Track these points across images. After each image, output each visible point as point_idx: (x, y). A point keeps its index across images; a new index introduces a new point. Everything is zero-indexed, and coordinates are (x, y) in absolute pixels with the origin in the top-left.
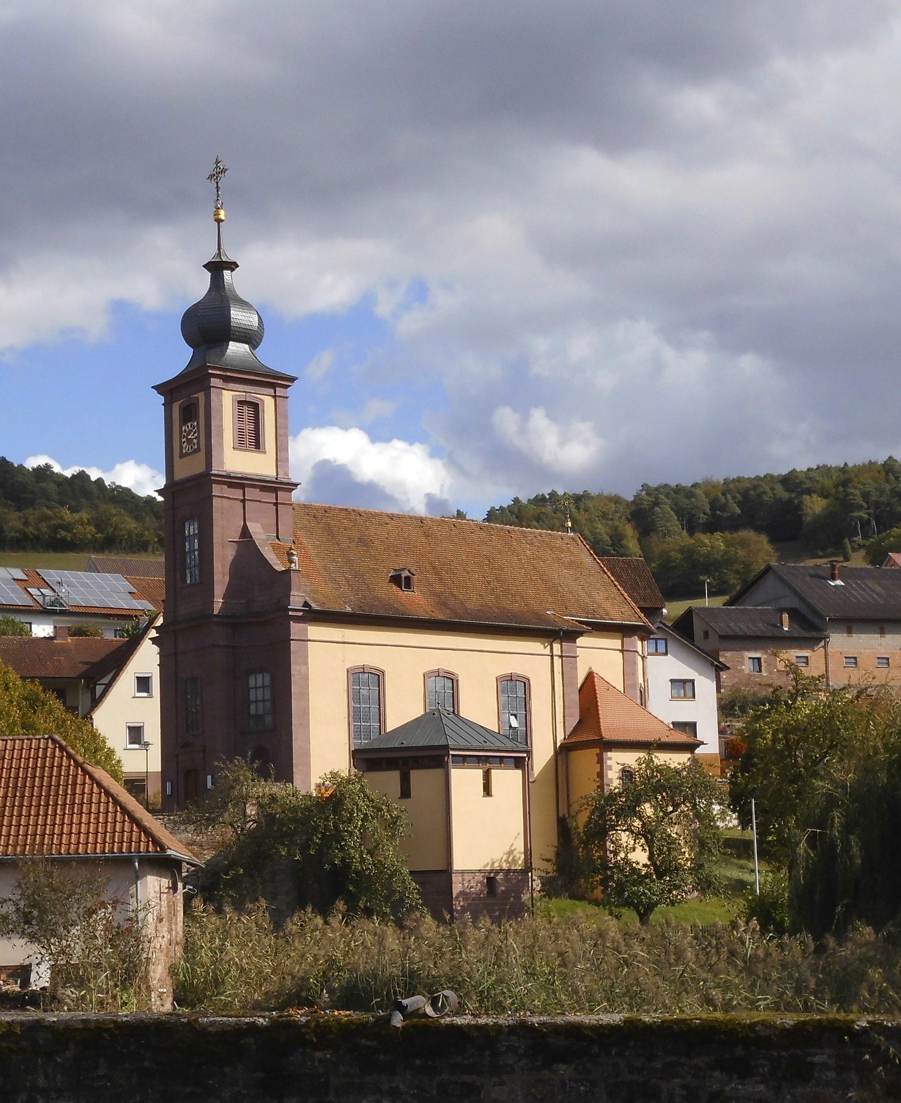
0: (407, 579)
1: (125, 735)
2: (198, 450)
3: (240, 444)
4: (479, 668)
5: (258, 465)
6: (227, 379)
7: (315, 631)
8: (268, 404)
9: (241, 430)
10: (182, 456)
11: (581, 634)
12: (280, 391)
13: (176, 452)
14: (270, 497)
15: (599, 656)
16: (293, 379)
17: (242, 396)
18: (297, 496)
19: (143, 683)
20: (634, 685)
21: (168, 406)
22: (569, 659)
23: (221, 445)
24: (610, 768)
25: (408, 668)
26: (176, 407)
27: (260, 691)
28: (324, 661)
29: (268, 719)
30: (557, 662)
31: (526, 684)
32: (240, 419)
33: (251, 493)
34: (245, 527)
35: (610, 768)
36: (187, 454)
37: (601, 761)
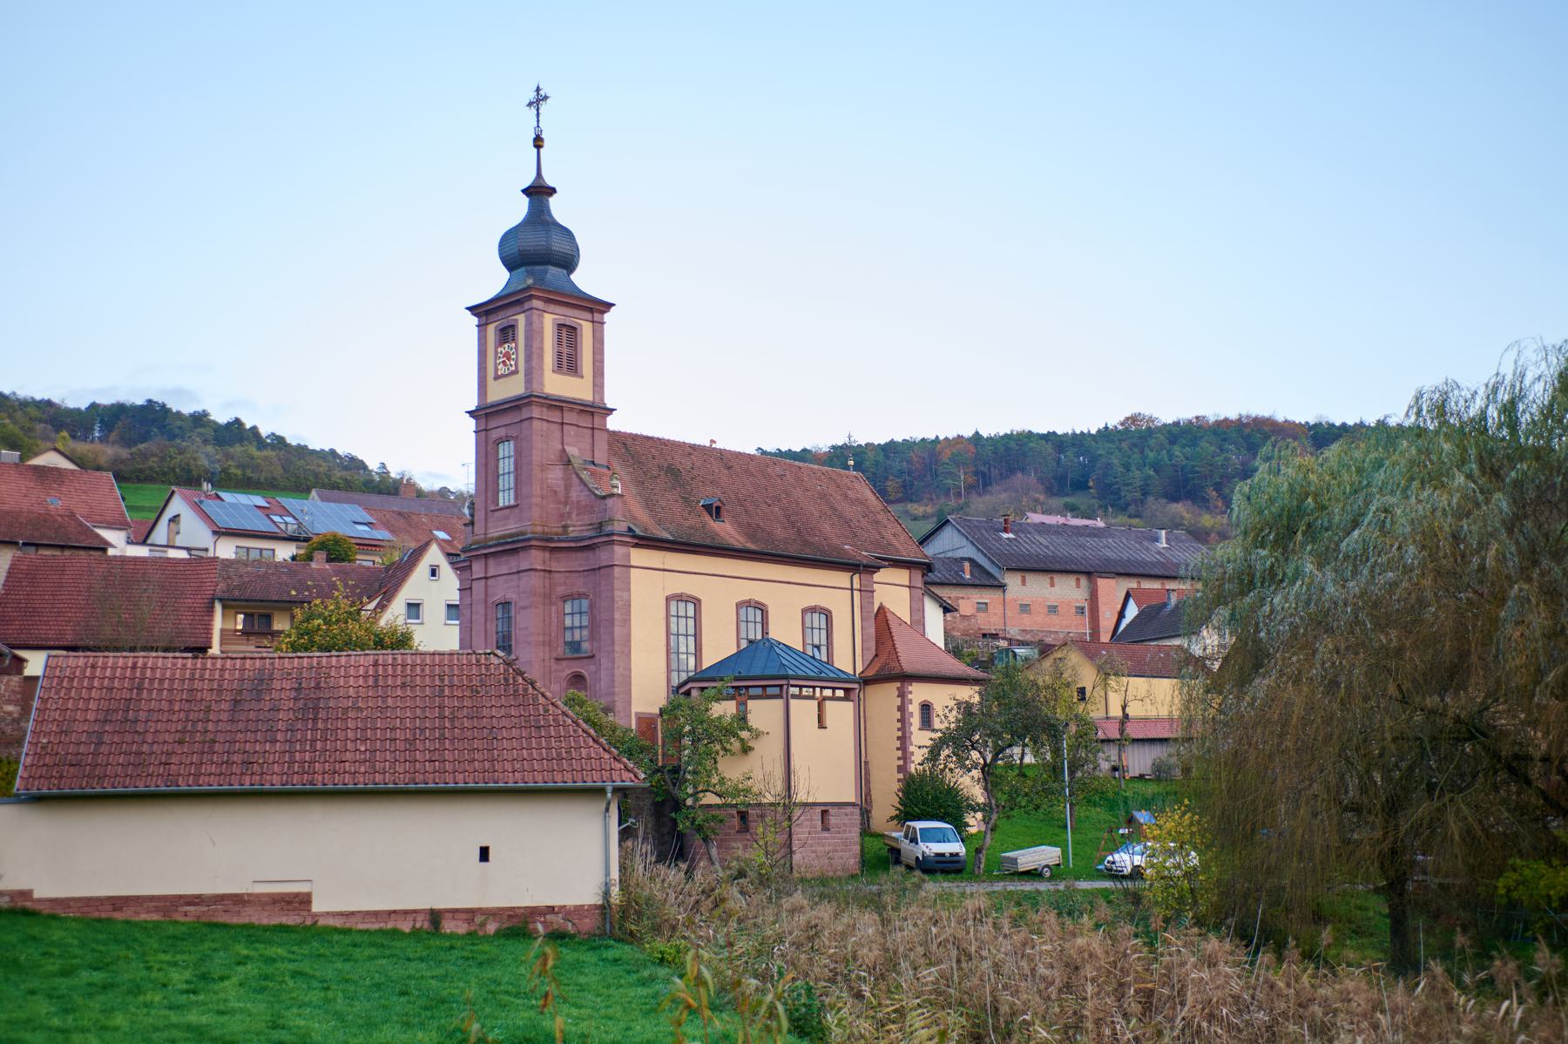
2: (516, 372)
4: (791, 602)
6: (548, 301)
7: (639, 556)
8: (586, 329)
9: (560, 354)
11: (878, 568)
12: (597, 317)
13: (491, 374)
14: (585, 421)
16: (610, 305)
17: (562, 320)
18: (613, 423)
21: (481, 327)
22: (867, 592)
23: (542, 369)
26: (491, 330)
27: (751, 618)
28: (649, 584)
29: (585, 646)
30: (857, 594)
31: (828, 614)
32: (560, 343)
33: (570, 417)
36: (503, 376)
37: (902, 694)
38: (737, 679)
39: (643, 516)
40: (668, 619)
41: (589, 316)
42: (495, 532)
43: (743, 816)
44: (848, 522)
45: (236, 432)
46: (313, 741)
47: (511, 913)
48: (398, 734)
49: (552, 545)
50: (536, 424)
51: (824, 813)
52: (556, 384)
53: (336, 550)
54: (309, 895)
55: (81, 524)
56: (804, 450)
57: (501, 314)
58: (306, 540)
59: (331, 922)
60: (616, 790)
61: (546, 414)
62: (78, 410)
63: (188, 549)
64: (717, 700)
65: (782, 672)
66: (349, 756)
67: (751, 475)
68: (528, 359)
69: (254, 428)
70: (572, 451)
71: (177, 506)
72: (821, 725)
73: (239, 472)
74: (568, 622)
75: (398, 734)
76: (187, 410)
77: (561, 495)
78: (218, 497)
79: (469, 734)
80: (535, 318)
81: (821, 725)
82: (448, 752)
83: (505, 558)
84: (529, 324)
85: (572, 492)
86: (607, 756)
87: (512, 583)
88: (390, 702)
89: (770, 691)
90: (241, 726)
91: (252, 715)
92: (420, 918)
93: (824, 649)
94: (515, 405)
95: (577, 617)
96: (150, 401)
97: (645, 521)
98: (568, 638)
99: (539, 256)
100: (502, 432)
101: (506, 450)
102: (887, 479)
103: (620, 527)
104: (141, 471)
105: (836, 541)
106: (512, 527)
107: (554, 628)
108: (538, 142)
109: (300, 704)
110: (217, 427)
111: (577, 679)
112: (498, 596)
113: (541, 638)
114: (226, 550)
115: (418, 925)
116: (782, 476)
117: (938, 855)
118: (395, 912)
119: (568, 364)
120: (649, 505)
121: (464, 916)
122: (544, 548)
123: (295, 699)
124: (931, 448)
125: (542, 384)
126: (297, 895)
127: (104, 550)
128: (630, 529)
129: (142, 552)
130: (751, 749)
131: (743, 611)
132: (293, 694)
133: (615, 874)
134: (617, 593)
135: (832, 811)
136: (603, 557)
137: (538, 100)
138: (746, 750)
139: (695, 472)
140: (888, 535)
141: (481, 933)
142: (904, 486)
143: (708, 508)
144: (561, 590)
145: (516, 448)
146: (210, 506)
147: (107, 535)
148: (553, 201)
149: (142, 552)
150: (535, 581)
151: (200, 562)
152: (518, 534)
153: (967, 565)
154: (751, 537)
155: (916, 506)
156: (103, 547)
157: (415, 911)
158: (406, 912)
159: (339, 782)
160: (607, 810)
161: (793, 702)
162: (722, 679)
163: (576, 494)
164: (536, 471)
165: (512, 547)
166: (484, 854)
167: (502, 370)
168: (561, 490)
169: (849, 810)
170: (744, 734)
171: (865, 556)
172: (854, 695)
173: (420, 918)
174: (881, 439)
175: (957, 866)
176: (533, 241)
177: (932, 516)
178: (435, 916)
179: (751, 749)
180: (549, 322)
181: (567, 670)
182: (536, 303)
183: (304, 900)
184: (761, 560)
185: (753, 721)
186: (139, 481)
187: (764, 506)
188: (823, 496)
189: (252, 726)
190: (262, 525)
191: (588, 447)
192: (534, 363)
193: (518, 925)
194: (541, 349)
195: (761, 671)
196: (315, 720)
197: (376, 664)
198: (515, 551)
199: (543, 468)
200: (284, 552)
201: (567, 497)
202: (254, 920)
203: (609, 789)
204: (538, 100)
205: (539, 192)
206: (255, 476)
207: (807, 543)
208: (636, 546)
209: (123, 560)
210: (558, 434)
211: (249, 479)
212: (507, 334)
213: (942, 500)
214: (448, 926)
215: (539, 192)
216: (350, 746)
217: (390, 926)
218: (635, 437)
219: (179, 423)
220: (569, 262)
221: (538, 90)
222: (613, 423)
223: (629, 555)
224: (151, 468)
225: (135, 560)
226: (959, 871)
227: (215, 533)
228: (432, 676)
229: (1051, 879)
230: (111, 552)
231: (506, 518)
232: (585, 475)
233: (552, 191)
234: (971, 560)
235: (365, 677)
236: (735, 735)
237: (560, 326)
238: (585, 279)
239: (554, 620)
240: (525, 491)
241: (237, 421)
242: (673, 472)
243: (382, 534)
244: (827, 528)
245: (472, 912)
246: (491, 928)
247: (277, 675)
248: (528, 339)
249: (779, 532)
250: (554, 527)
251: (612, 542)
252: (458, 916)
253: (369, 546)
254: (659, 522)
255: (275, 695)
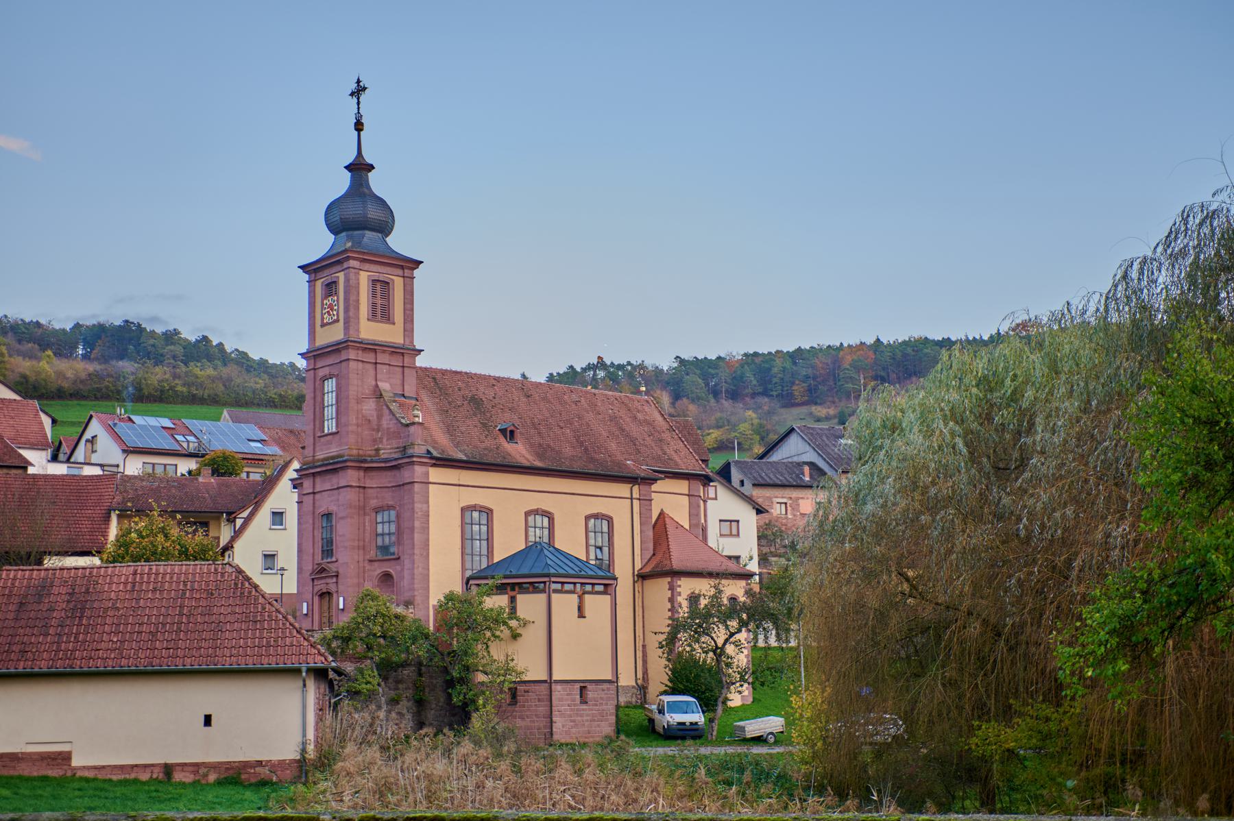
0: (506, 429)
1: (260, 560)
2: (337, 321)
3: (373, 317)
4: (573, 515)
5: (389, 334)
7: (435, 474)
8: (398, 283)
9: (374, 305)
10: (323, 325)
11: (655, 480)
13: (318, 322)
14: (396, 361)
15: (671, 500)
16: (418, 263)
17: (376, 276)
18: (420, 361)
19: (278, 516)
20: (697, 525)
22: (646, 501)
24: (680, 594)
25: (515, 511)
27: (539, 524)
28: (444, 500)
30: (636, 503)
31: (610, 520)
32: (374, 295)
33: (382, 358)
34: (377, 386)
35: (680, 594)
38: (505, 577)
39: (442, 439)
40: (451, 529)
41: (400, 272)
42: (320, 455)
43: (514, 693)
44: (633, 441)
45: (203, 350)
46: (77, 634)
47: (228, 766)
48: (144, 628)
49: (365, 465)
50: (351, 363)
51: (583, 689)
52: (369, 331)
53: (222, 466)
54: (69, 753)
55: (7, 446)
56: (719, 358)
57: (326, 272)
58: (203, 456)
59: (87, 774)
60: (309, 670)
61: (361, 355)
62: (64, 330)
63: (101, 466)
64: (488, 595)
65: (546, 571)
66: (103, 645)
67: (549, 402)
68: (347, 310)
69: (221, 344)
70: (384, 386)
71: (95, 428)
72: (581, 615)
73: (185, 389)
74: (380, 530)
75: (144, 628)
76: (159, 329)
77: (375, 423)
78: (130, 420)
79: (200, 627)
80: (352, 276)
81: (581, 615)
82: (213, 642)
83: (328, 477)
84: (347, 280)
85: (376, 422)
86: (306, 643)
87: (339, 497)
88: (142, 603)
89: (567, 587)
90: (23, 623)
91: (32, 614)
92: (156, 770)
93: (606, 550)
94: (336, 348)
95: (386, 526)
96: (127, 321)
97: (444, 443)
98: (380, 542)
99: (359, 219)
100: (326, 371)
101: (330, 385)
102: (793, 383)
103: (419, 450)
104: (99, 390)
105: (620, 457)
106: (333, 450)
107: (367, 535)
108: (359, 126)
109: (71, 606)
110: (187, 345)
111: (387, 578)
112: (322, 509)
113: (356, 544)
114: (134, 467)
115: (155, 776)
116: (576, 403)
117: (679, 724)
118: (136, 766)
119: (382, 313)
120: (450, 430)
121: (191, 769)
122: (359, 468)
123: (68, 602)
124: (835, 352)
125: (358, 331)
126: (60, 753)
127: (25, 468)
128: (428, 452)
129: (60, 469)
130: (520, 635)
131: (531, 519)
132: (67, 597)
133: (311, 735)
134: (417, 506)
135: (589, 687)
136: (406, 475)
137: (359, 91)
138: (515, 636)
139: (496, 401)
140: (670, 451)
141: (203, 782)
142: (810, 390)
143: (503, 431)
144: (374, 503)
145: (338, 384)
146: (122, 428)
147: (28, 454)
148: (372, 176)
149: (60, 469)
150: (349, 496)
151: (111, 476)
152: (338, 456)
153: (806, 469)
154: (540, 456)
155: (819, 408)
156: (24, 465)
157: (153, 765)
158: (146, 766)
159: (92, 666)
160: (305, 685)
161: (554, 596)
162: (493, 577)
163: (386, 422)
164: (353, 404)
165: (333, 467)
166: (208, 720)
167: (327, 319)
168: (374, 419)
169: (605, 686)
170: (513, 623)
171: (644, 470)
172: (610, 590)
173: (156, 770)
174: (790, 347)
175: (696, 733)
176: (352, 211)
177: (835, 417)
178: (168, 769)
179: (520, 635)
180: (364, 278)
181: (378, 569)
182: (352, 263)
183: (66, 757)
184: (547, 475)
185: (520, 613)
186: (96, 399)
187: (556, 429)
188: (613, 419)
189: (31, 623)
190: (166, 443)
191: (399, 382)
192: (351, 314)
193: (235, 776)
194: (358, 301)
195: (532, 573)
196: (81, 618)
197: (135, 573)
198: (335, 471)
199: (359, 401)
200: (185, 466)
201: (379, 425)
202: (26, 773)
203: (304, 669)
204: (359, 91)
205: (359, 168)
206: (199, 393)
207: (592, 460)
208: (434, 465)
209: (46, 478)
210: (372, 372)
211: (194, 396)
212: (330, 288)
213: (843, 404)
214: (178, 776)
215: (359, 168)
216: (105, 637)
217: (133, 776)
218: (444, 372)
219: (152, 341)
220: (385, 227)
221: (358, 82)
222: (420, 361)
223: (427, 474)
224: (107, 387)
225: (54, 477)
226: (700, 737)
227: (124, 451)
228: (178, 583)
229: (776, 743)
230: (31, 470)
231: (329, 443)
232: (394, 406)
233: (371, 167)
234: (812, 465)
235: (125, 584)
236: (505, 623)
237: (375, 281)
238: (398, 242)
239: (368, 528)
240: (343, 420)
241: (205, 338)
242: (476, 402)
243: (268, 450)
244: (613, 446)
245: (197, 765)
246: (212, 777)
247: (57, 582)
248: (347, 293)
249: (568, 451)
250: (368, 450)
251: (413, 463)
252: (186, 768)
253: (256, 460)
254: (457, 445)
255: (52, 598)
